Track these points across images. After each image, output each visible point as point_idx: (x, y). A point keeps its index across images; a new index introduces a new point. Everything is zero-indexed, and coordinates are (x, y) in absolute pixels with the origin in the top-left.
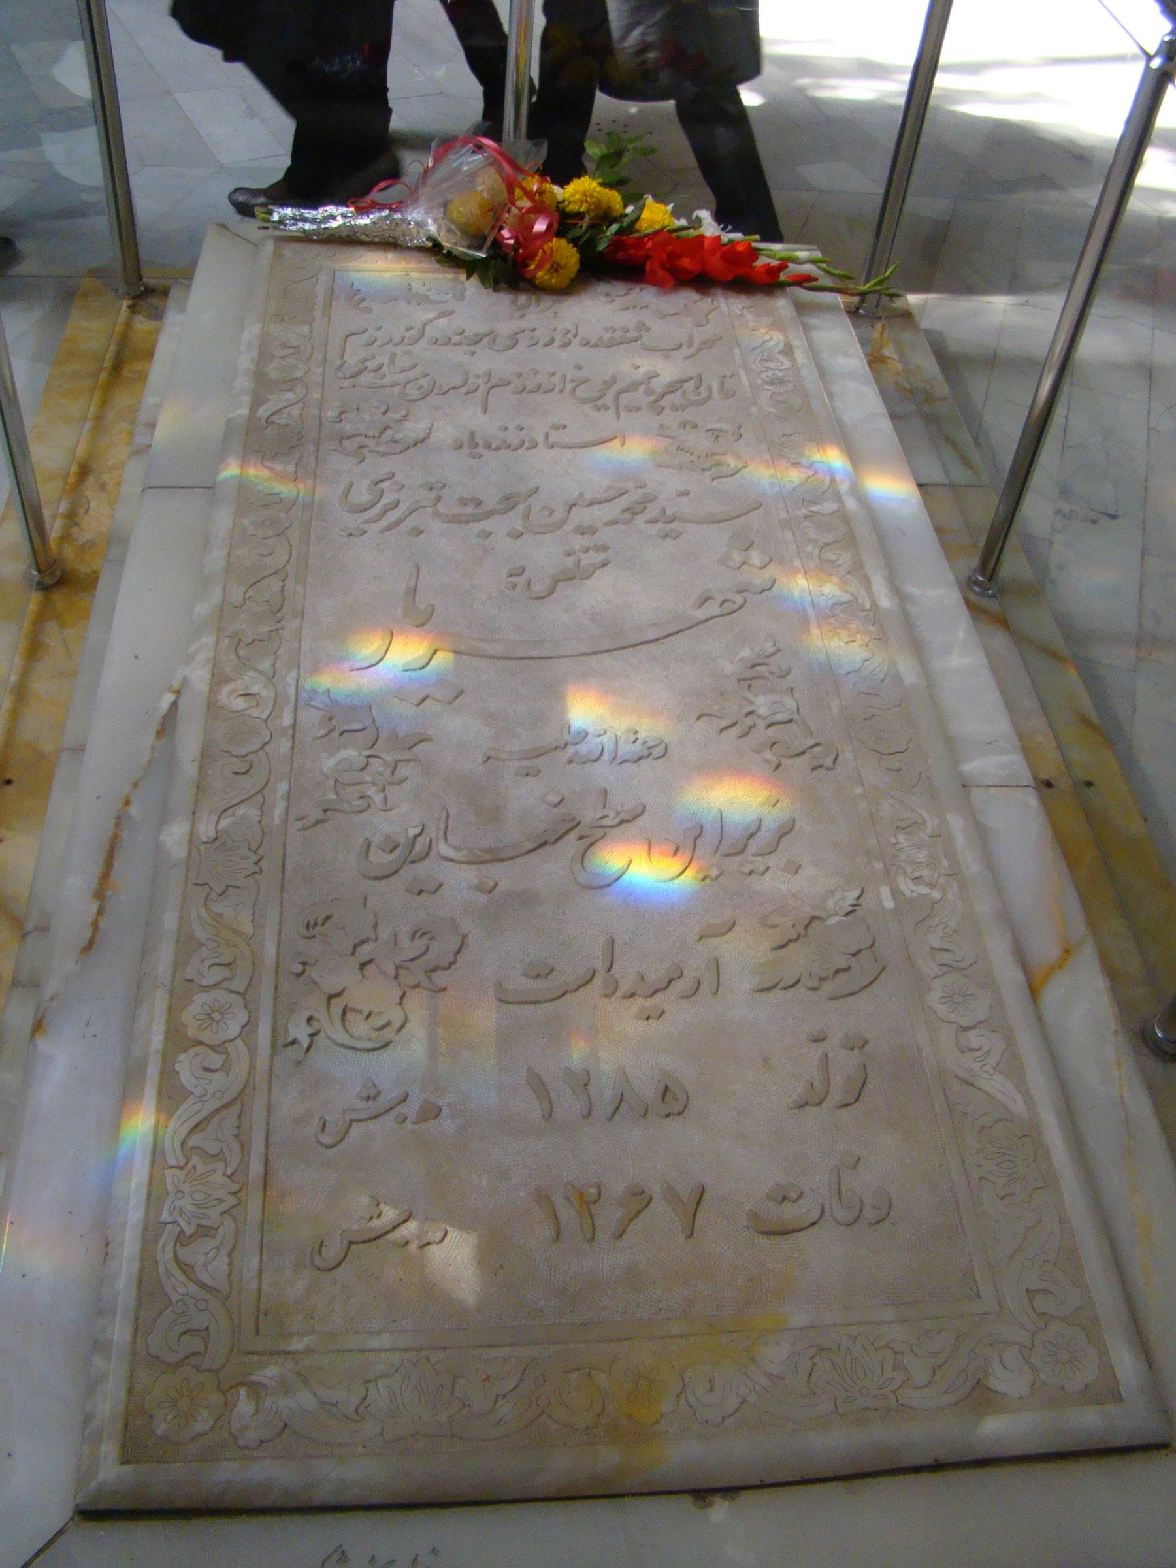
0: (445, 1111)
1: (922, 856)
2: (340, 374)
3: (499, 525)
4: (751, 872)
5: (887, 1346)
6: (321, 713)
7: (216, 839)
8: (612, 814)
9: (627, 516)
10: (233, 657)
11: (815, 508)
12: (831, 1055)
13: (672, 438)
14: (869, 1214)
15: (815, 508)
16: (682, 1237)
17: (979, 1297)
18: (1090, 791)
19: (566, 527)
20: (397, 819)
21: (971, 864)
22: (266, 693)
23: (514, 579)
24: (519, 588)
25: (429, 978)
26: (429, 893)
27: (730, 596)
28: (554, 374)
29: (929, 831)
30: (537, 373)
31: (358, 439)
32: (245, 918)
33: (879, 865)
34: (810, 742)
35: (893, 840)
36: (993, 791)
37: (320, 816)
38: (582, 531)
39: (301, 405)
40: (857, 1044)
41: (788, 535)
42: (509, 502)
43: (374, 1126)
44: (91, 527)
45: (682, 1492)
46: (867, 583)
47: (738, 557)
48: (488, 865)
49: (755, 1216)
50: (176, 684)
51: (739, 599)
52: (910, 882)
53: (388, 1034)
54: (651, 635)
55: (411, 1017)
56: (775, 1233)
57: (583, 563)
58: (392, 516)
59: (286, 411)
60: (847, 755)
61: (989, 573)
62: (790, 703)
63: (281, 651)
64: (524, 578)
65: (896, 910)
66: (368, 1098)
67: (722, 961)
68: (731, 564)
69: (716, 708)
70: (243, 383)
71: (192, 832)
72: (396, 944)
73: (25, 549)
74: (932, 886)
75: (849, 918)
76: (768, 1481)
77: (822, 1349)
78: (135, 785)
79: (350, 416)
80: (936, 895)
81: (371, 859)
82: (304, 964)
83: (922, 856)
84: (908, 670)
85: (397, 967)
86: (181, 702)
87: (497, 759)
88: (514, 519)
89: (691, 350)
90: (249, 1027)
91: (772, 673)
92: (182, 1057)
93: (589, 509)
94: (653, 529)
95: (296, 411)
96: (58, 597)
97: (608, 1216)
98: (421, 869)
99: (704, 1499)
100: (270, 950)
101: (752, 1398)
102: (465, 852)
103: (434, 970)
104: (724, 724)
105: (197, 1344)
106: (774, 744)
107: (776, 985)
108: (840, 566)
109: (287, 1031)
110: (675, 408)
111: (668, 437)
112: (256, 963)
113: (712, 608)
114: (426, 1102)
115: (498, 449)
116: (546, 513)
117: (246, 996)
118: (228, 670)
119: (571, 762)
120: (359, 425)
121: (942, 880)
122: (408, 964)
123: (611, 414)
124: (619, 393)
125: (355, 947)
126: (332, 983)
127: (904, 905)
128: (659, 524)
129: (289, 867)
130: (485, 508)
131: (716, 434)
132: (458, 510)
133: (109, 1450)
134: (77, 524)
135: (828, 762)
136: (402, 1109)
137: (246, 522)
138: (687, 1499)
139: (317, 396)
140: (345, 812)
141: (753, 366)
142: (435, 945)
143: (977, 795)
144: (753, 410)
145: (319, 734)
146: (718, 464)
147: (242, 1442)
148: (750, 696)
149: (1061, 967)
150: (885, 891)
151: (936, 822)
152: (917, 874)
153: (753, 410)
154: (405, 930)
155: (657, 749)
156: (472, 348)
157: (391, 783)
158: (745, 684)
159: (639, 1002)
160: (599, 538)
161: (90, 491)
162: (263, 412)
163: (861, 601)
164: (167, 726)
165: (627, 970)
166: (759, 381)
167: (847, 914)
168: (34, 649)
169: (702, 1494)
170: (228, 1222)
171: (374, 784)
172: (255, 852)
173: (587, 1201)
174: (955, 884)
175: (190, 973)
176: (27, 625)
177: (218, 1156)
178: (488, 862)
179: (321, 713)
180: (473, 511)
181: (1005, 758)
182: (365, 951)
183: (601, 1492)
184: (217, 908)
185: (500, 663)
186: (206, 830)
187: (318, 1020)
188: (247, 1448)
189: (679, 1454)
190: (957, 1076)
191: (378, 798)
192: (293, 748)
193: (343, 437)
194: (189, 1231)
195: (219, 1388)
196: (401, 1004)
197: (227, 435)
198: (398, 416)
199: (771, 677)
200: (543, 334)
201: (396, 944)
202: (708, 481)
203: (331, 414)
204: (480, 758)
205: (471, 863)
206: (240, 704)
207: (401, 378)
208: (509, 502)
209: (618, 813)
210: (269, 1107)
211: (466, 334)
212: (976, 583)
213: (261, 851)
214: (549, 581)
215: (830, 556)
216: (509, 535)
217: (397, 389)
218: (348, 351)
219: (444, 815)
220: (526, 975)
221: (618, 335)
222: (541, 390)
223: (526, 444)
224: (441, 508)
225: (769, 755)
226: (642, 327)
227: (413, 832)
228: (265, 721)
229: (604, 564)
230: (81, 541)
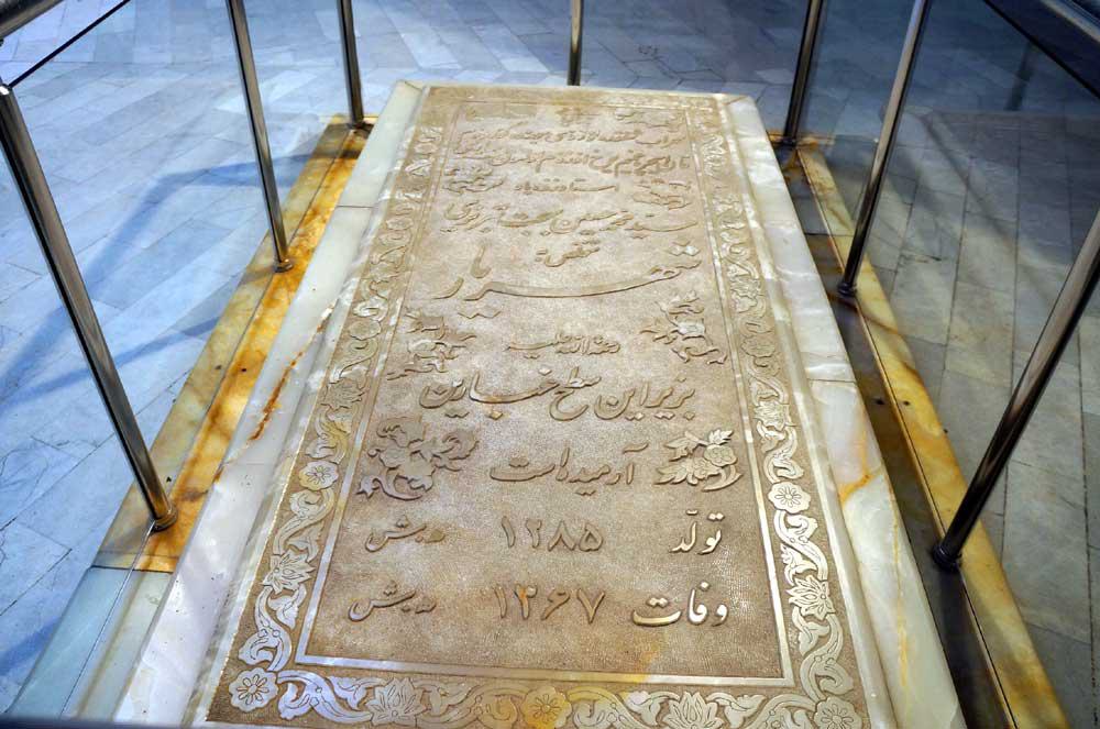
3: (537, 228)
10: (368, 289)
18: (907, 407)
34: (711, 348)
37: (402, 372)
42: (544, 216)
46: (758, 265)
47: (679, 249)
51: (677, 271)
52: (765, 429)
53: (420, 492)
58: (472, 223)
66: (402, 526)
82: (378, 450)
87: (515, 349)
88: (546, 227)
90: (339, 481)
92: (294, 495)
94: (628, 233)
95: (427, 169)
98: (457, 405)
104: (657, 336)
105: (267, 655)
110: (651, 172)
112: (350, 447)
117: (341, 469)
118: (364, 295)
123: (612, 175)
124: (619, 164)
126: (390, 462)
137: (388, 222)
139: (442, 162)
143: (816, 386)
147: (282, 716)
149: (862, 485)
153: (700, 174)
154: (441, 435)
158: (674, 316)
160: (596, 237)
162: (407, 169)
164: (324, 326)
165: (576, 464)
167: (721, 444)
170: (302, 587)
180: (521, 222)
181: (838, 365)
182: (414, 447)
186: (334, 377)
188: (285, 719)
194: (278, 591)
197: (387, 180)
200: (578, 134)
206: (367, 313)
214: (560, 257)
224: (504, 219)
227: (456, 384)
229: (597, 250)
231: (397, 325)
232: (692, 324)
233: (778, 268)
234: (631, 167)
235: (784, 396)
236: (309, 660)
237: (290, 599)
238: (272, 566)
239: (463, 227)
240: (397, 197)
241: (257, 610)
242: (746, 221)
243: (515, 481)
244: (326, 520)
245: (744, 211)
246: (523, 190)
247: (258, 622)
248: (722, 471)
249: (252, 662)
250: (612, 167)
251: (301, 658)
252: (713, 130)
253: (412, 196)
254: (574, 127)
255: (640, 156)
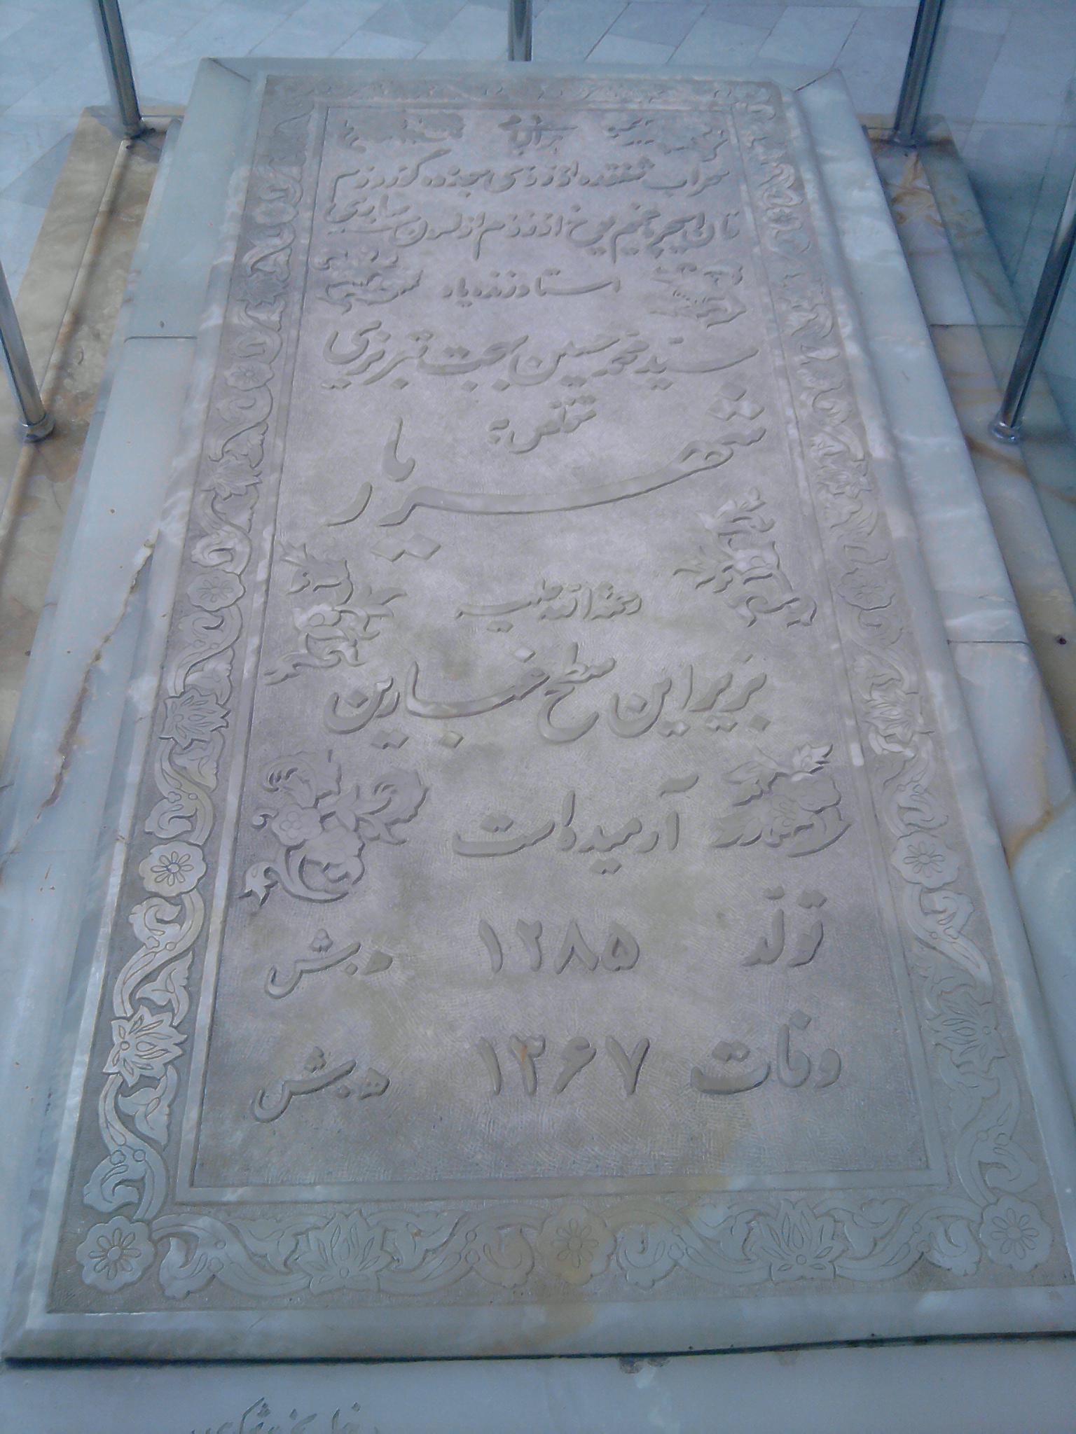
0: (395, 962)
1: (896, 713)
2: (329, 219)
4: (718, 728)
5: (827, 1214)
6: (295, 568)
7: (183, 694)
8: (581, 669)
9: (617, 366)
10: (209, 511)
11: (813, 355)
12: (788, 913)
13: (669, 282)
14: (817, 1077)
15: (813, 355)
16: (624, 1093)
17: (927, 1167)
19: (555, 379)
20: (369, 673)
21: (949, 722)
22: (242, 549)
23: (498, 433)
24: (502, 442)
25: (389, 830)
26: (394, 747)
27: (718, 448)
28: (551, 215)
29: (906, 687)
30: (533, 215)
31: (344, 287)
32: (209, 771)
33: (850, 723)
34: (788, 597)
35: (867, 697)
36: (981, 646)
37: (290, 670)
38: (569, 382)
39: (288, 251)
40: (814, 901)
41: (782, 383)
42: (497, 352)
43: (323, 976)
44: (83, 380)
45: (611, 1355)
46: (861, 431)
48: (455, 720)
49: (699, 1074)
50: (152, 538)
51: (725, 452)
52: (881, 740)
53: (344, 885)
54: (633, 491)
55: (369, 869)
56: (719, 1093)
57: (569, 416)
58: (376, 368)
59: (273, 257)
60: (827, 609)
61: (1011, 420)
62: (770, 558)
63: (257, 506)
64: (508, 430)
65: (866, 768)
66: (320, 949)
67: (683, 817)
68: (720, 415)
69: (694, 562)
70: (230, 228)
71: (160, 686)
72: (358, 796)
73: (13, 401)
74: (904, 744)
75: (815, 775)
76: (696, 1348)
77: (760, 1214)
78: (107, 640)
79: (339, 263)
80: (909, 753)
81: (339, 712)
83: (896, 713)
84: (898, 526)
85: (358, 820)
86: (155, 557)
88: (501, 371)
89: (697, 187)
91: (753, 527)
92: (136, 908)
93: (578, 360)
95: (282, 258)
96: (47, 449)
97: (551, 1069)
98: (387, 724)
99: (632, 1364)
100: (232, 800)
101: (684, 1261)
102: (432, 706)
103: (394, 823)
104: (700, 579)
106: (750, 599)
107: (735, 842)
108: (835, 414)
109: (244, 885)
111: (665, 281)
112: (218, 815)
113: (696, 462)
114: (378, 953)
115: (488, 296)
116: (534, 363)
117: (208, 851)
118: (203, 524)
119: (543, 617)
120: (346, 273)
121: (916, 738)
122: (369, 818)
123: (607, 258)
125: (317, 800)
126: (289, 835)
127: (873, 763)
128: (649, 375)
129: (255, 721)
130: (469, 360)
131: (714, 277)
132: (443, 361)
133: (37, 1298)
134: (71, 376)
135: (805, 617)
136: (353, 960)
137: (227, 373)
138: (615, 1362)
140: (315, 667)
141: (761, 204)
142: (397, 799)
143: (962, 652)
144: (756, 250)
145: (294, 589)
146: (715, 310)
147: (168, 1293)
148: (728, 550)
150: (855, 749)
151: (914, 678)
152: (890, 732)
155: (632, 604)
156: (467, 189)
157: (363, 639)
159: (596, 856)
161: (83, 341)
162: (248, 259)
163: (853, 450)
164: (141, 581)
165: (585, 825)
166: (765, 219)
168: (24, 501)
169: (629, 1358)
170: (171, 1070)
171: (346, 639)
172: (222, 706)
173: (531, 1053)
174: (930, 742)
175: (150, 826)
176: (16, 478)
177: (168, 1008)
178: (455, 716)
179: (295, 568)
180: (460, 362)
182: (326, 805)
183: (524, 1353)
184: (180, 761)
185: (478, 518)
186: (174, 683)
187: (276, 872)
188: (174, 1298)
189: (608, 1318)
190: (918, 939)
191: (349, 654)
192: (266, 603)
193: (329, 286)
194: (131, 1081)
195: (150, 1238)
196: (359, 856)
198: (387, 262)
199: (753, 531)
201: (358, 796)
202: (703, 327)
203: (318, 260)
204: (454, 613)
205: (436, 717)
206: (214, 559)
207: (392, 222)
208: (497, 352)
209: (587, 669)
210: (220, 961)
211: (461, 174)
212: (998, 430)
213: (228, 706)
214: (533, 435)
215: (825, 404)
216: (494, 387)
217: (387, 234)
218: (339, 193)
219: (414, 670)
220: (484, 828)
221: (619, 172)
222: (537, 233)
223: (517, 292)
224: (428, 358)
225: (744, 610)
226: (645, 163)
227: (381, 687)
228: (239, 576)
230: (74, 392)
231: (268, 580)
232: (756, 552)
233: (896, 432)
234: (638, 238)
235: (909, 679)
236: (199, 1194)
237: (153, 1094)
238: (116, 1039)
239: (358, 380)
240: (235, 320)
241: (102, 1120)
242: (839, 343)
243: (494, 855)
244: (196, 949)
245: (834, 325)
246: (455, 298)
247: (107, 1139)
248: (816, 820)
249: (106, 1207)
250: (605, 242)
251: (184, 1192)
252: (777, 154)
253: (262, 316)
254: (531, 155)
255: (654, 215)
